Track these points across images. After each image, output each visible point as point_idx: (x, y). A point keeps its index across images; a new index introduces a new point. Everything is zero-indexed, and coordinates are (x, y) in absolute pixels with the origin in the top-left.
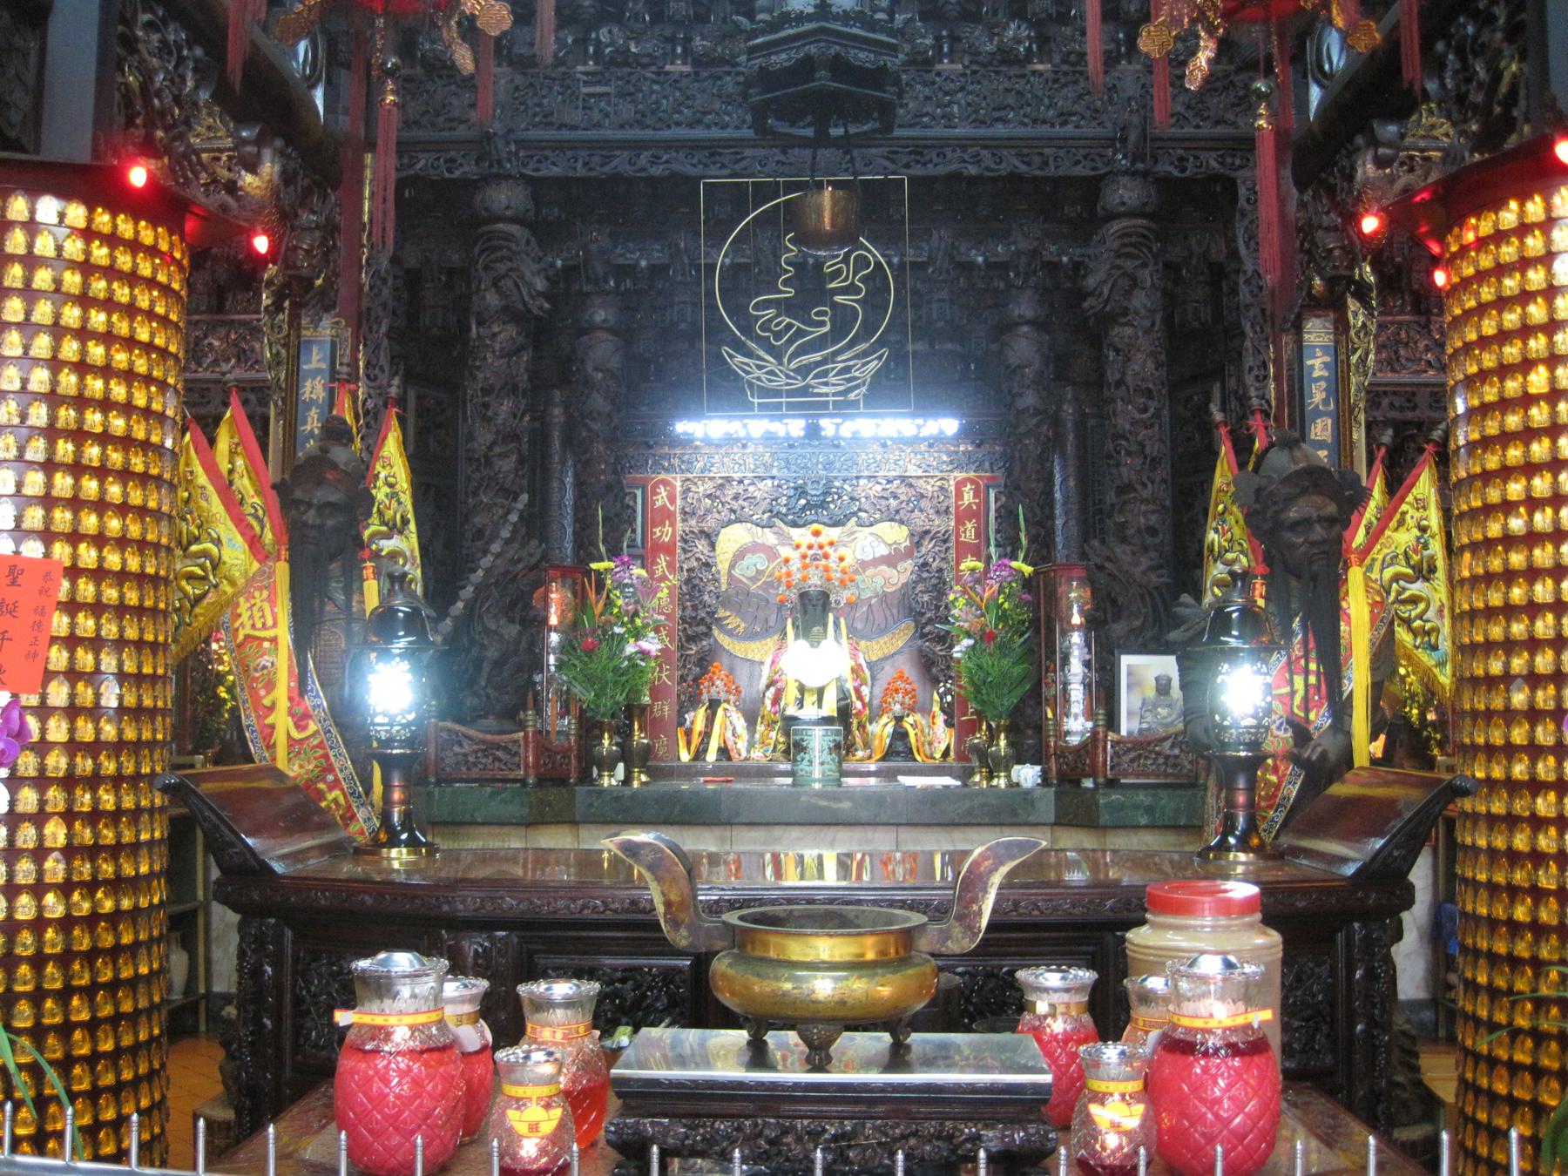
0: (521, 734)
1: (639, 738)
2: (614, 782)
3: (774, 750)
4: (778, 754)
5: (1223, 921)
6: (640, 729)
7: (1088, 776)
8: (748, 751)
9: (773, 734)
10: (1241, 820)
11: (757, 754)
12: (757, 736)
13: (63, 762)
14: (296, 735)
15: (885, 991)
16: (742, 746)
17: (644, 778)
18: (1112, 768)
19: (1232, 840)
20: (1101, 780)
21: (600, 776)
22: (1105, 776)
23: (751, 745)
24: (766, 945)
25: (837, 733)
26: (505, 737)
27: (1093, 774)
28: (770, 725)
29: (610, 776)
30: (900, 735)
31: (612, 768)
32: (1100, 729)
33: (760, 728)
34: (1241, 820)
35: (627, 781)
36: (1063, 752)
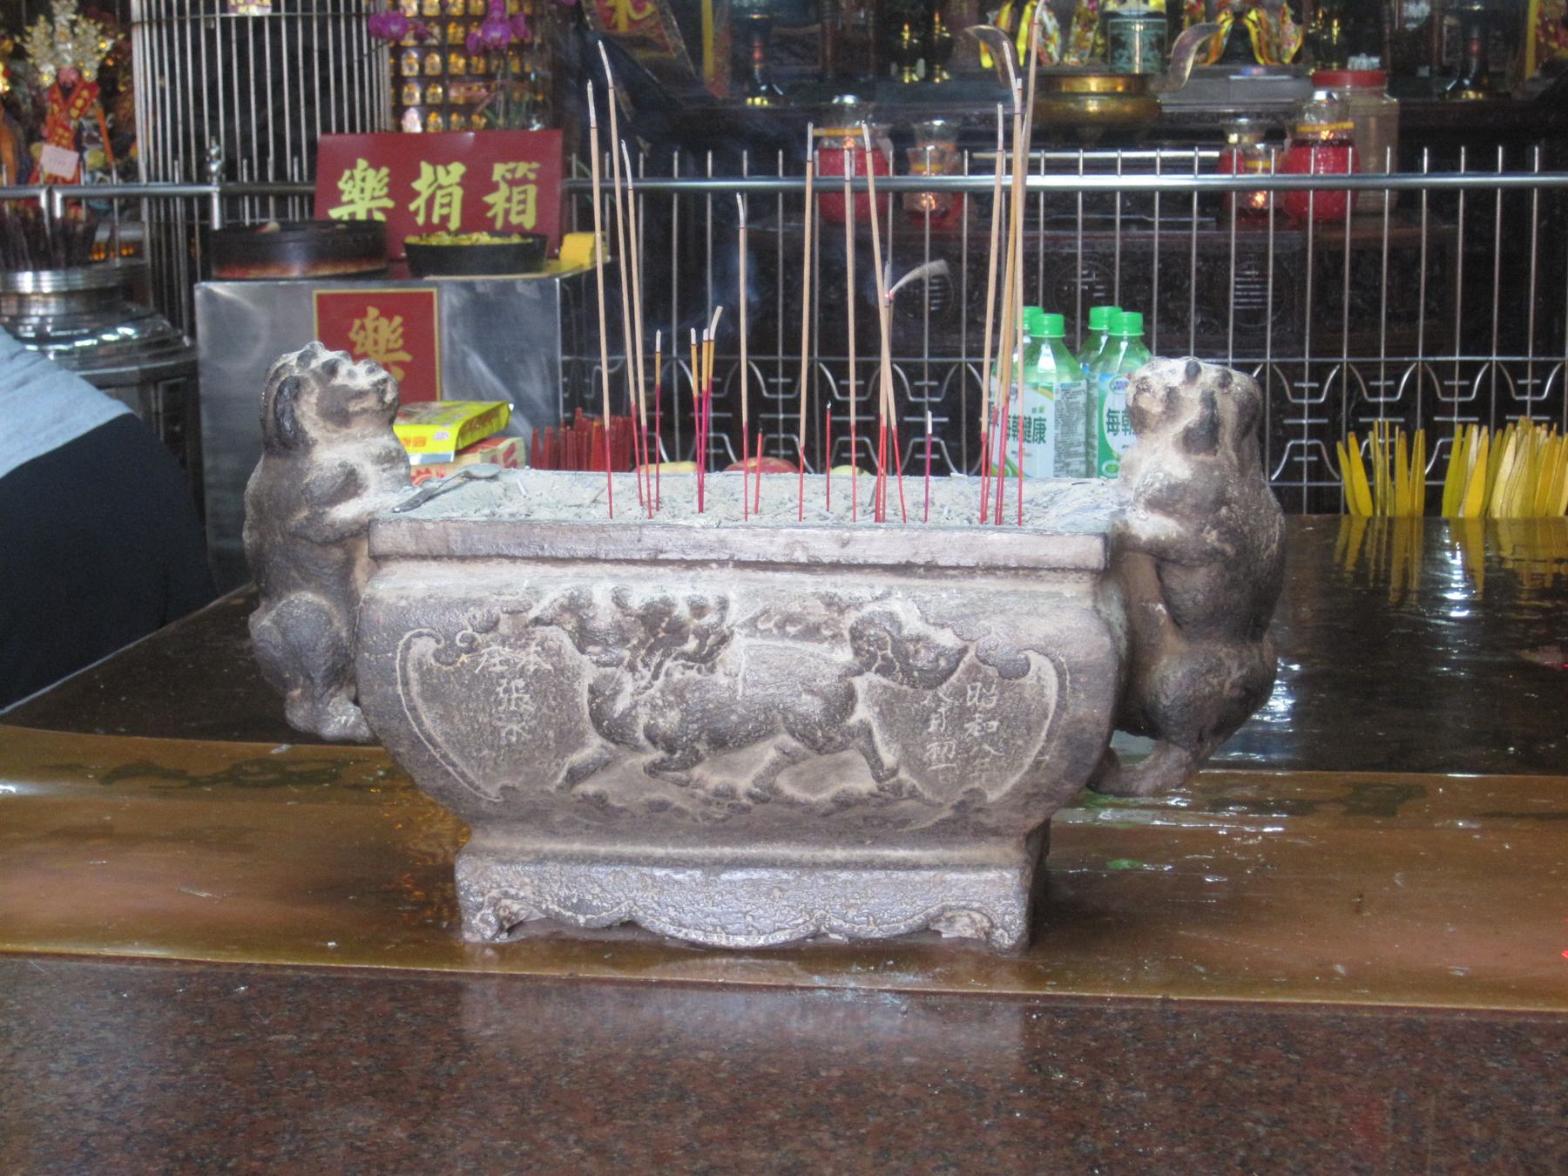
0: (818, 27)
1: (941, 31)
2: (915, 78)
3: (1092, 54)
4: (1097, 60)
5: (1359, 89)
6: (942, 22)
7: (1424, 64)
8: (1061, 57)
9: (1090, 35)
10: (1474, 62)
11: (1071, 60)
12: (1072, 39)
13: (460, 31)
14: (636, 16)
15: (1128, 109)
16: (1053, 49)
17: (945, 76)
18: (1448, 54)
19: (1467, 82)
20: (1436, 68)
21: (901, 72)
22: (1440, 63)
23: (1064, 49)
24: (1059, 85)
25: (1161, 26)
26: (801, 31)
27: (1428, 62)
28: (1087, 25)
29: (912, 72)
30: (1239, 33)
31: (913, 63)
32: (1437, 14)
33: (1076, 29)
34: (1474, 62)
35: (929, 76)
36: (1400, 37)
